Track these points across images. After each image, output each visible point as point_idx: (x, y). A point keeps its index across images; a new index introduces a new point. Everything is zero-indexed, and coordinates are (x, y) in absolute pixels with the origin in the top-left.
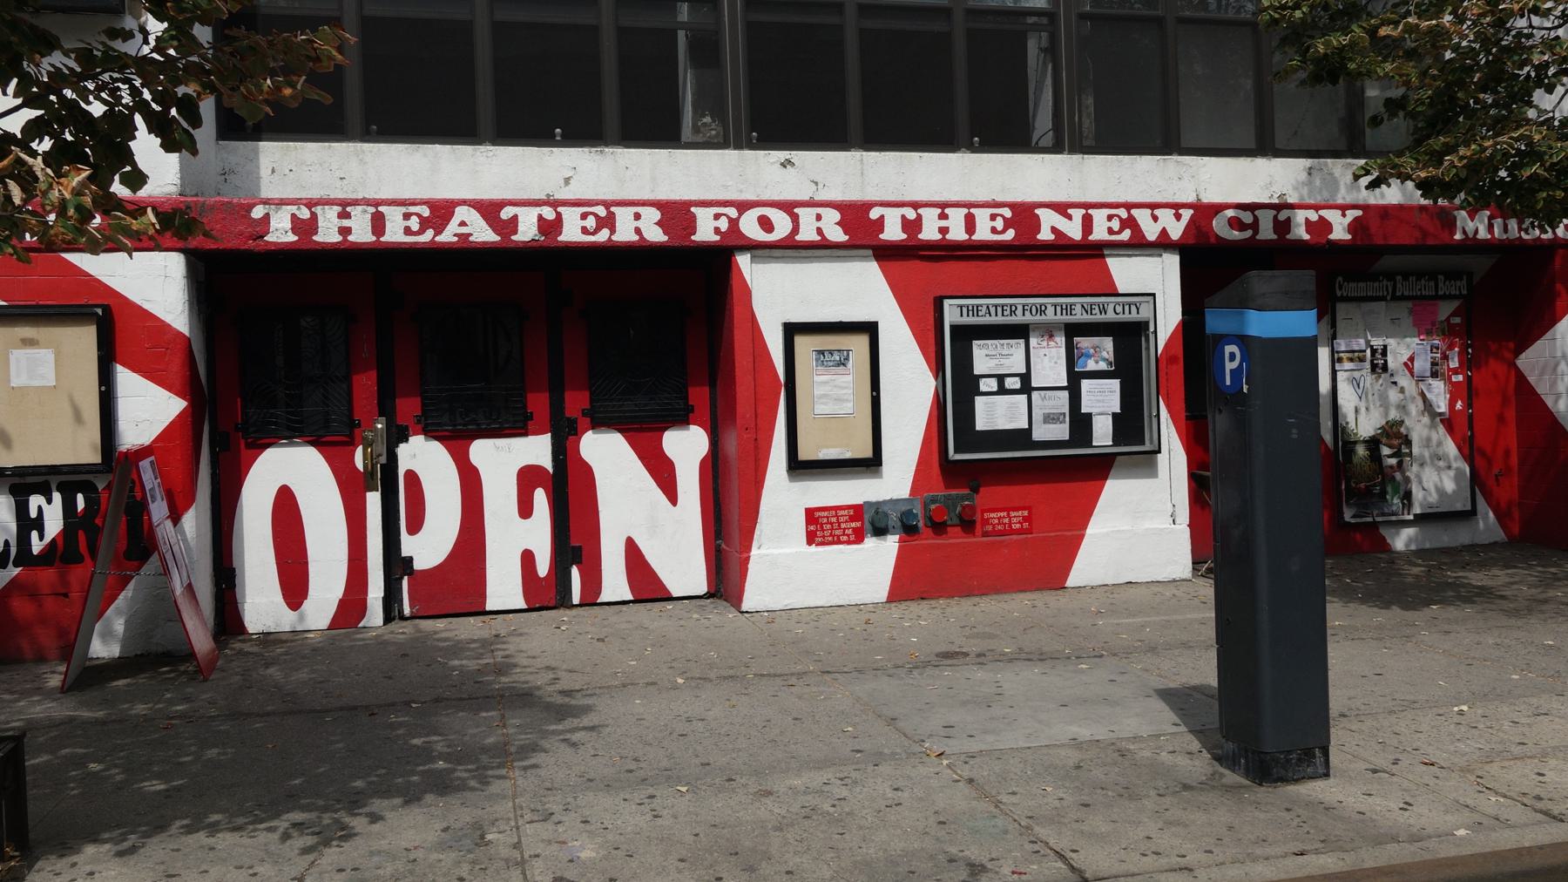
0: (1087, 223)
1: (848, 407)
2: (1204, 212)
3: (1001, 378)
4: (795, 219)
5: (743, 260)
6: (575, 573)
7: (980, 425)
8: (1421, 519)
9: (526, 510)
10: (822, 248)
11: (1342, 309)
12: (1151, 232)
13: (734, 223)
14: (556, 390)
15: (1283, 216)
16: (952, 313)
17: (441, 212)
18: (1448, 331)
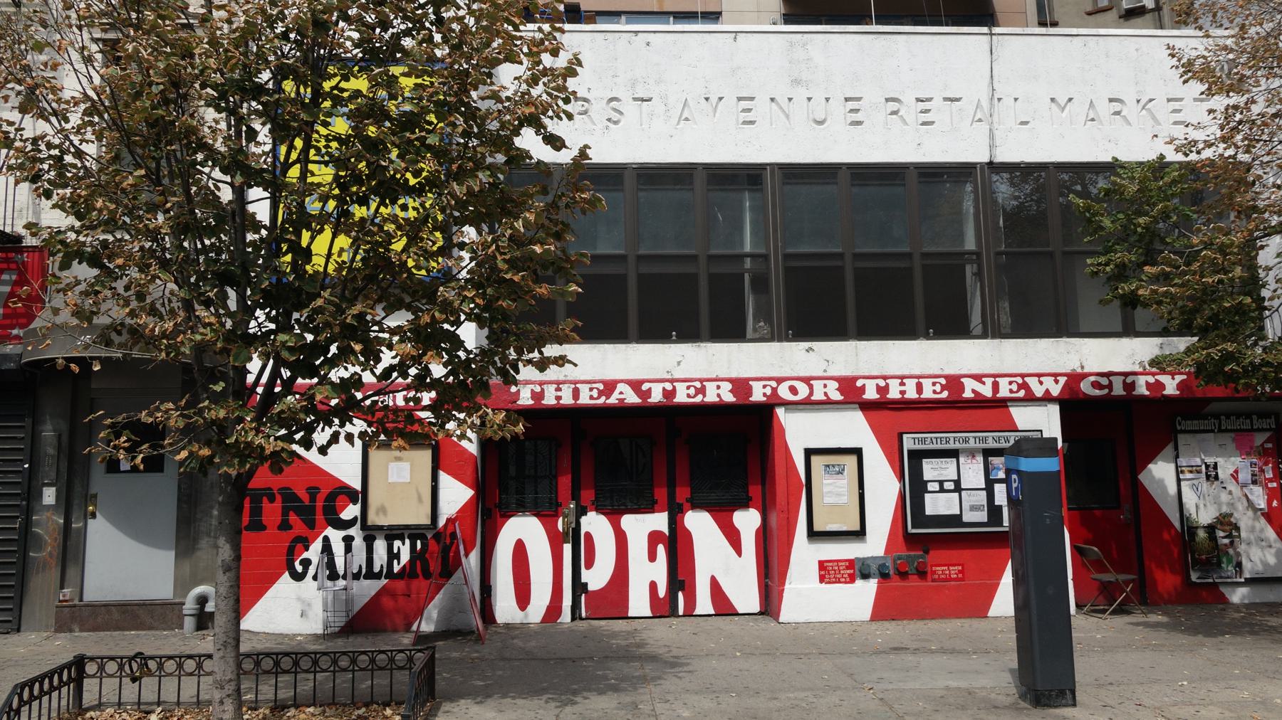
0: (996, 387)
1: (844, 499)
2: (1075, 378)
3: (941, 483)
4: (811, 387)
5: (780, 412)
6: (680, 595)
7: (929, 511)
8: (1250, 582)
9: (652, 557)
10: (827, 403)
11: (1182, 439)
12: (1039, 391)
13: (774, 390)
14: (672, 485)
15: (1129, 380)
16: (909, 442)
17: (610, 386)
18: (1263, 453)
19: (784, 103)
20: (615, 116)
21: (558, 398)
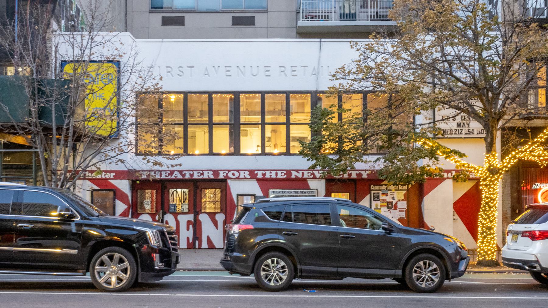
0: (303, 174)
4: (239, 173)
5: (229, 181)
6: (197, 241)
9: (188, 229)
17: (172, 172)
19: (242, 68)
20: (181, 74)
21: (271, 176)
